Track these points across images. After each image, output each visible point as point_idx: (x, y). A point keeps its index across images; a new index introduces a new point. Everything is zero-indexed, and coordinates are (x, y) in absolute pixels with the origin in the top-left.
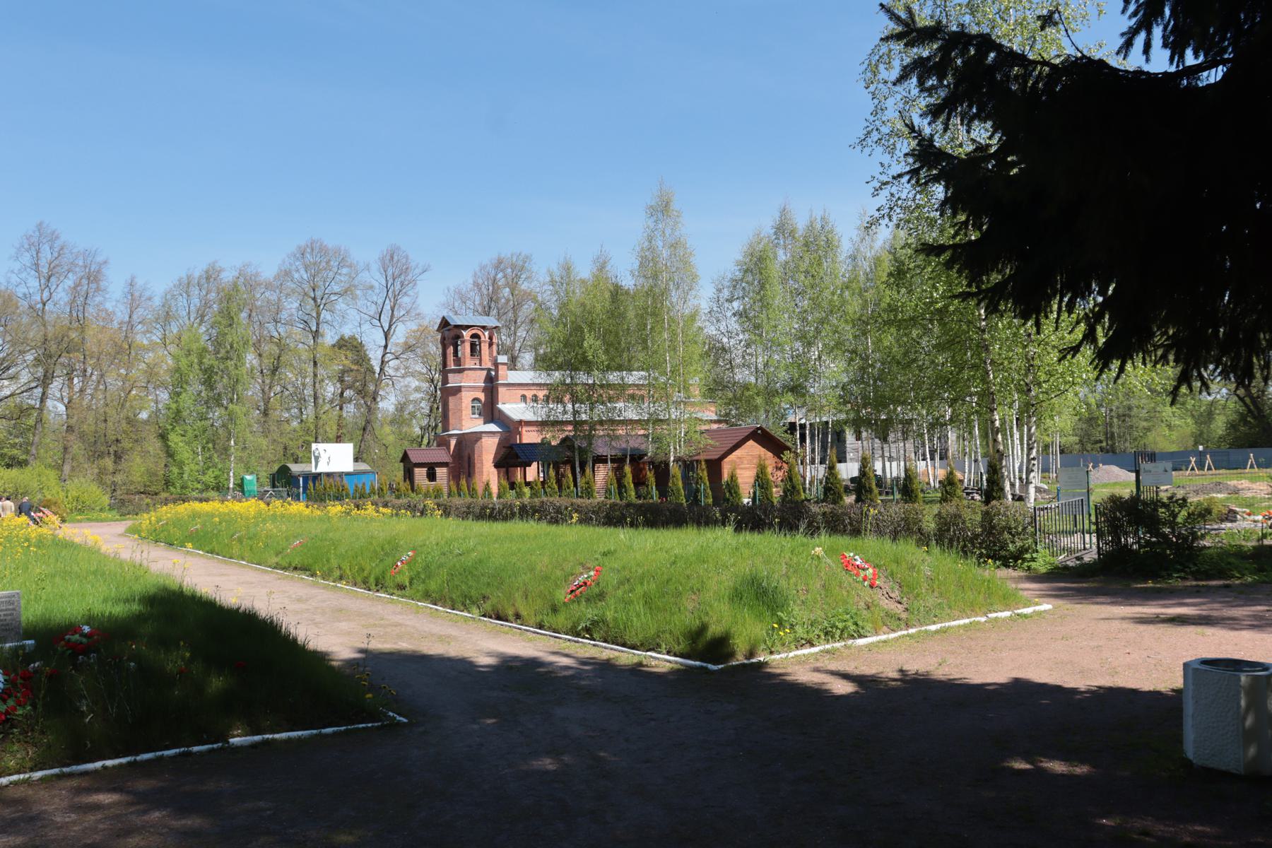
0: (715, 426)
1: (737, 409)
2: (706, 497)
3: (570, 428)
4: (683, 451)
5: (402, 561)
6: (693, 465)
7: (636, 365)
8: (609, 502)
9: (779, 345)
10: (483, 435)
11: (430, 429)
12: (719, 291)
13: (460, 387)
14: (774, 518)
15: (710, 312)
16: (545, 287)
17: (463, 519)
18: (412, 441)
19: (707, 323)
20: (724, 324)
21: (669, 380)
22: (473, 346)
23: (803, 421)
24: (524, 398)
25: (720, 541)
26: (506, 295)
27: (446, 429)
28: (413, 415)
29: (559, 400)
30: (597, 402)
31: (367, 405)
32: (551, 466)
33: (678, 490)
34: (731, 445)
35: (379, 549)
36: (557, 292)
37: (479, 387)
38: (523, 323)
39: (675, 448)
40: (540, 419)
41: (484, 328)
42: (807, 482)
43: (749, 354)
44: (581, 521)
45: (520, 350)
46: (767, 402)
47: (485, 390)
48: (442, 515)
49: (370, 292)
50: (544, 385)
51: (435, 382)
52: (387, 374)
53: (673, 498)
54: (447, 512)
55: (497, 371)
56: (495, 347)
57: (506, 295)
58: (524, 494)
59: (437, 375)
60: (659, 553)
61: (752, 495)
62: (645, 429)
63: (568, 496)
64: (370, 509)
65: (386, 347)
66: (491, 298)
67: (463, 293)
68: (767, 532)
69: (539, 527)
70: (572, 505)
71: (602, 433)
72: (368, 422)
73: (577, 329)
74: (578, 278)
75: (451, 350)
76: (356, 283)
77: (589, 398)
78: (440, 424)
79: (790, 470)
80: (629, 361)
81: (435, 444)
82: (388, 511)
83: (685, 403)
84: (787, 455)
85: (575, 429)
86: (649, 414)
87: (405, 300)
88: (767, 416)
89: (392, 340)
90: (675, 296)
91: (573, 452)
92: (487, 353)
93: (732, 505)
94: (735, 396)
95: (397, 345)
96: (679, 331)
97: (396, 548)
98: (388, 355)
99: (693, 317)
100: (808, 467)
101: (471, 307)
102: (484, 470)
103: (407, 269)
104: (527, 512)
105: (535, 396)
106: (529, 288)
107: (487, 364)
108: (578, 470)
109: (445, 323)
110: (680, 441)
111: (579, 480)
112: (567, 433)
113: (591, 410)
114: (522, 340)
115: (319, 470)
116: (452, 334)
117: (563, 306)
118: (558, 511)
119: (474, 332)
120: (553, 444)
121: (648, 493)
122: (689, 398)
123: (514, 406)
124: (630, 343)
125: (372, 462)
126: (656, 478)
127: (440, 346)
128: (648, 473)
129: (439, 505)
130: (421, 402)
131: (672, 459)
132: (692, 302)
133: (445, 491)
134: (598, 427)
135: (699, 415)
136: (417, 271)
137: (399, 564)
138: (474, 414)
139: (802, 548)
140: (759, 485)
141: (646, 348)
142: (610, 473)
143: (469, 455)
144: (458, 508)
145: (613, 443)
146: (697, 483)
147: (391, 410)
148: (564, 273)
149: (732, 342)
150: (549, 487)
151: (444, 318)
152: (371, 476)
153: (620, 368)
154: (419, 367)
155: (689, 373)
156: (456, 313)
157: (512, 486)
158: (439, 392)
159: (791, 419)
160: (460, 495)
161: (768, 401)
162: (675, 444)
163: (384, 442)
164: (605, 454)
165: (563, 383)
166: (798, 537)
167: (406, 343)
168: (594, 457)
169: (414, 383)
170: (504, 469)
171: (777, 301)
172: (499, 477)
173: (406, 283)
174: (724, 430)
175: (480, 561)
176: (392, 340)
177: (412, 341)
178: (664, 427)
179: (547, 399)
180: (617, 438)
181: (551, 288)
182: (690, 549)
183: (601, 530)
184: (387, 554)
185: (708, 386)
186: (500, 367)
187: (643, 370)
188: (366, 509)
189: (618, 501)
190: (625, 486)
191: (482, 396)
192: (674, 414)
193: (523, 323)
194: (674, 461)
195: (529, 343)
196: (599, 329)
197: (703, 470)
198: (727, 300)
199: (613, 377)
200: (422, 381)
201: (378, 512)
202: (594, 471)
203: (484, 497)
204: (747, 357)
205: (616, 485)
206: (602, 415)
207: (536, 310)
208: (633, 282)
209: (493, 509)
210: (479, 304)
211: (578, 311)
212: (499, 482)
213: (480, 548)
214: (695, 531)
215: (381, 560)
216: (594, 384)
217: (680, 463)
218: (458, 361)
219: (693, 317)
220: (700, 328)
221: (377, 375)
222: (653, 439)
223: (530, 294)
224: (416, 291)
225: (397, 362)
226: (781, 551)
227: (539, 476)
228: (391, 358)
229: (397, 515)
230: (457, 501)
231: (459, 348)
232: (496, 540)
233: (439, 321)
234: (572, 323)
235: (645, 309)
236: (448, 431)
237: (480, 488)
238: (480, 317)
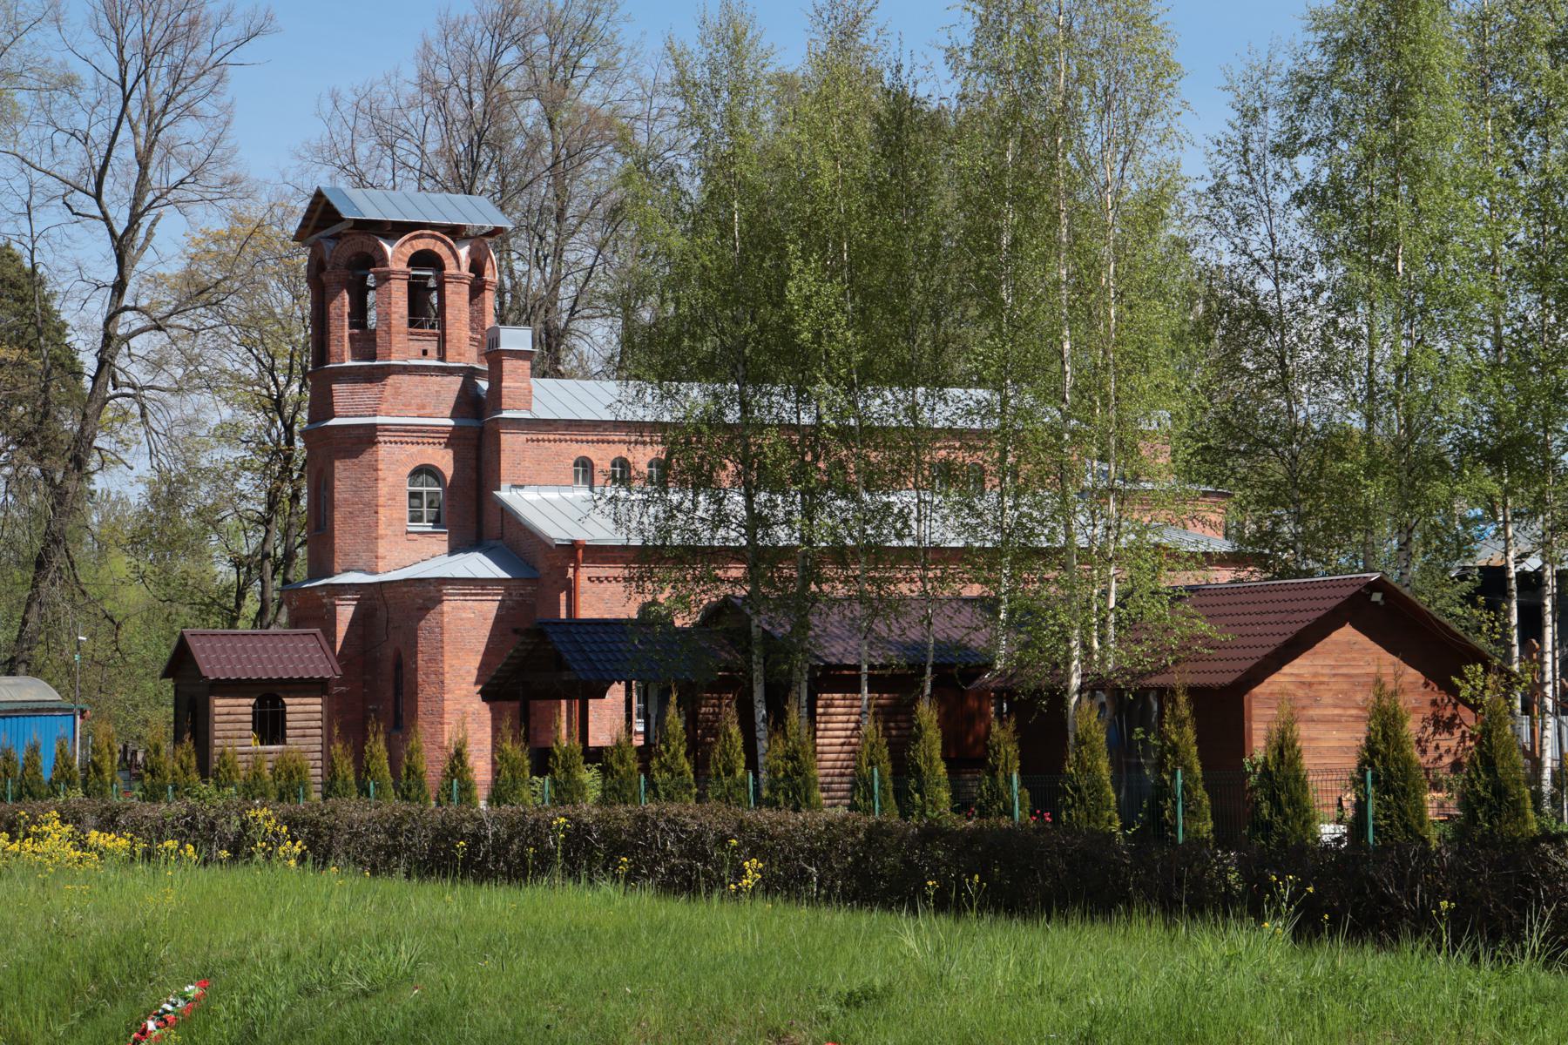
0: (1224, 576)
1: (1300, 519)
2: (1191, 814)
3: (736, 571)
4: (1113, 658)
5: (162, 1019)
6: (1147, 706)
7: (960, 367)
8: (864, 821)
9: (1454, 302)
10: (448, 589)
11: (268, 567)
12: (1251, 116)
13: (374, 426)
14: (1437, 894)
15: (1214, 190)
16: (659, 101)
17: (374, 872)
18: (207, 607)
19: (1201, 229)
20: (1263, 230)
21: (1067, 417)
22: (417, 292)
23: (1533, 564)
24: (585, 468)
25: (1245, 968)
26: (529, 122)
27: (322, 564)
28: (209, 519)
29: (702, 480)
30: (828, 486)
31: (50, 481)
32: (674, 698)
33: (1097, 788)
34: (1279, 640)
35: (80, 975)
36: (696, 121)
37: (433, 431)
38: (583, 219)
39: (1086, 647)
40: (636, 541)
41: (455, 233)
42: (1547, 775)
43: (1346, 334)
44: (769, 887)
45: (573, 311)
46: (1403, 498)
47: (454, 440)
48: (302, 859)
49: (65, 98)
50: (657, 426)
51: (289, 410)
52: (122, 378)
53: (1078, 814)
54: (319, 851)
55: (496, 377)
56: (490, 299)
57: (529, 122)
58: (580, 788)
59: (295, 387)
60: (1037, 1002)
61: (1350, 814)
62: (986, 582)
63: (726, 798)
64: (56, 833)
65: (119, 287)
66: (481, 133)
67: (385, 113)
68: (1407, 946)
69: (631, 901)
70: (740, 828)
71: (841, 591)
72: (54, 539)
73: (764, 240)
74: (770, 70)
75: (342, 303)
76: (15, 65)
77: (800, 474)
78: (302, 552)
79: (1486, 733)
80: (938, 352)
81: (283, 618)
82: (118, 843)
83: (1122, 498)
84: (1474, 680)
85: (753, 577)
86: (999, 528)
87: (185, 132)
88: (1404, 546)
89: (145, 265)
90: (1093, 133)
91: (747, 652)
92: (465, 316)
93: (1283, 843)
94: (1292, 475)
95: (157, 281)
96: (1106, 252)
97: (143, 971)
98: (129, 315)
99: (1153, 210)
100: (1551, 722)
101: (412, 160)
102: (449, 705)
103: (193, 23)
104: (590, 853)
105: (622, 464)
106: (606, 100)
107: (465, 354)
108: (761, 711)
109: (321, 213)
110: (1104, 622)
111: (763, 745)
112: (725, 589)
113: (808, 514)
114: (581, 276)
116: (347, 250)
117: (718, 168)
118: (694, 847)
119: (421, 245)
120: (678, 623)
121: (996, 795)
122: (1136, 478)
123: (552, 495)
124: (940, 292)
125: (65, 676)
126: (1022, 744)
127: (304, 288)
128: (996, 728)
129: (292, 822)
130: (236, 476)
131: (1075, 682)
132: (1151, 157)
133: (315, 773)
134: (829, 571)
135: (1169, 538)
136: (228, 33)
137: (151, 1025)
139: (1538, 1009)
140: (1376, 780)
141: (993, 308)
142: (868, 726)
143: (398, 655)
144: (357, 835)
145: (880, 627)
146: (1160, 765)
147: (134, 500)
148: (722, 56)
149: (1289, 292)
150: (663, 766)
151: (319, 195)
152: (61, 725)
153: (905, 376)
154: (235, 360)
155: (1135, 395)
156: (361, 181)
157: (542, 761)
158: (299, 444)
159: (1488, 554)
160: (364, 791)
161: (1409, 495)
162: (1086, 626)
163: (108, 606)
164: (851, 661)
165: (713, 422)
166: (1521, 968)
167: (189, 277)
168: (813, 668)
169: (216, 412)
170: (516, 705)
171: (1451, 153)
172: (496, 730)
173: (191, 71)
174: (1252, 590)
175: (433, 1017)
176: (140, 266)
177: (210, 272)
178: (1050, 574)
179: (662, 475)
180: (896, 606)
181: (680, 104)
182: (1144, 995)
183: (837, 918)
184: (110, 993)
185: (1200, 439)
186: (508, 365)
187: (981, 383)
188: (40, 837)
189: (893, 817)
190: (918, 769)
191: (444, 460)
192: (1085, 531)
193: (583, 219)
194: (1080, 691)
195: (604, 287)
196: (838, 245)
197: (1181, 723)
198: (1277, 149)
199: (883, 405)
200: (244, 406)
201: (83, 845)
202: (812, 715)
203: (445, 795)
204: (1341, 346)
205: (888, 767)
206: (841, 531)
207: (626, 179)
208: (955, 87)
209: (476, 839)
210: (439, 153)
211: (769, 183)
212: (496, 747)
213: (430, 971)
214: (1157, 930)
215: (89, 1014)
216: (818, 426)
217: (1103, 697)
218: (366, 342)
219: (1153, 210)
220: (1182, 245)
221: (87, 383)
222: (1011, 613)
223: (608, 123)
224: (225, 100)
225: (157, 339)
226: (1463, 1015)
227: (629, 729)
228: (138, 325)
229: (148, 855)
230: (354, 810)
231: (371, 297)
232: (488, 946)
233: (302, 206)
234: (750, 221)
235: (993, 179)
236: (331, 575)
237: (432, 767)
238: (441, 197)
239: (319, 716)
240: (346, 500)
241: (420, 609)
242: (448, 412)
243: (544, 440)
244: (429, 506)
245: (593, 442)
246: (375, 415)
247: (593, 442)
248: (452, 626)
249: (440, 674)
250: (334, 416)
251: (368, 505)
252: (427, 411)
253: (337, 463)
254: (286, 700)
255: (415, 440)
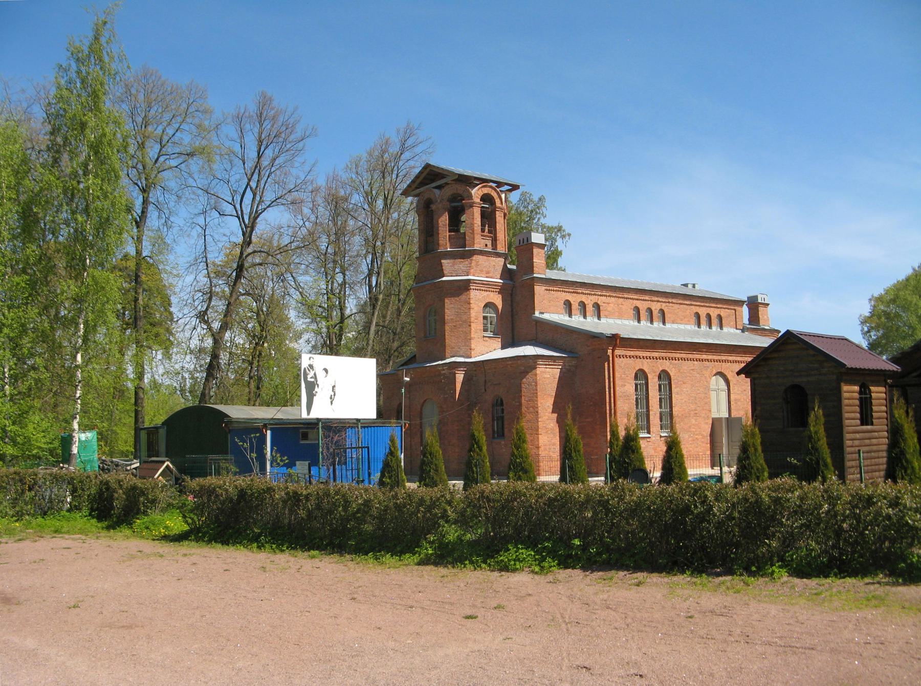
13: (469, 280)
37: (494, 284)
47: (502, 290)
115: (315, 414)
119: (486, 191)
138: (485, 330)
191: (498, 300)
239: (884, 395)
240: (452, 319)
241: (521, 373)
242: (499, 276)
243: (551, 290)
244: (491, 324)
245: (571, 292)
246: (468, 275)
247: (571, 292)
248: (541, 382)
249: (535, 408)
250: (443, 276)
251: (465, 321)
252: (490, 275)
253: (446, 301)
254: (872, 388)
255: (486, 289)
